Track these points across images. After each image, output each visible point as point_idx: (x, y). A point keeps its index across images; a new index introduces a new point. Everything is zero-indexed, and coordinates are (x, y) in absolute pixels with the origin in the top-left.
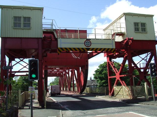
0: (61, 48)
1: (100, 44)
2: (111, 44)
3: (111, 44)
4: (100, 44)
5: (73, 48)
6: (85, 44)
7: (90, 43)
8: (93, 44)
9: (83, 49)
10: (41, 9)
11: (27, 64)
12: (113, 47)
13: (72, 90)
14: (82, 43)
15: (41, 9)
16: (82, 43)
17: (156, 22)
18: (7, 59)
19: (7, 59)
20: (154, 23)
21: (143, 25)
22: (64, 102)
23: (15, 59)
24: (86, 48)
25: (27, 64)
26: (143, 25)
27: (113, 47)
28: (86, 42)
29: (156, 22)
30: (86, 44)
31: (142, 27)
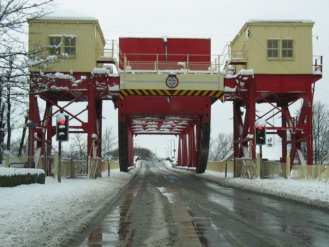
0: (126, 90)
1: (149, 82)
2: (216, 83)
3: (216, 83)
4: (149, 82)
5: (146, 90)
6: (168, 84)
7: (177, 82)
8: (182, 82)
9: (162, 91)
10: (310, 25)
11: (274, 106)
12: (219, 88)
13: (287, 126)
14: (162, 82)
15: (310, 25)
16: (162, 82)
17: (317, 38)
18: (42, 104)
19: (42, 104)
20: (314, 39)
21: (288, 44)
22: (127, 142)
23: (58, 102)
24: (168, 90)
25: (274, 106)
26: (288, 44)
27: (219, 88)
28: (170, 80)
29: (317, 38)
30: (168, 82)
31: (271, 47)
